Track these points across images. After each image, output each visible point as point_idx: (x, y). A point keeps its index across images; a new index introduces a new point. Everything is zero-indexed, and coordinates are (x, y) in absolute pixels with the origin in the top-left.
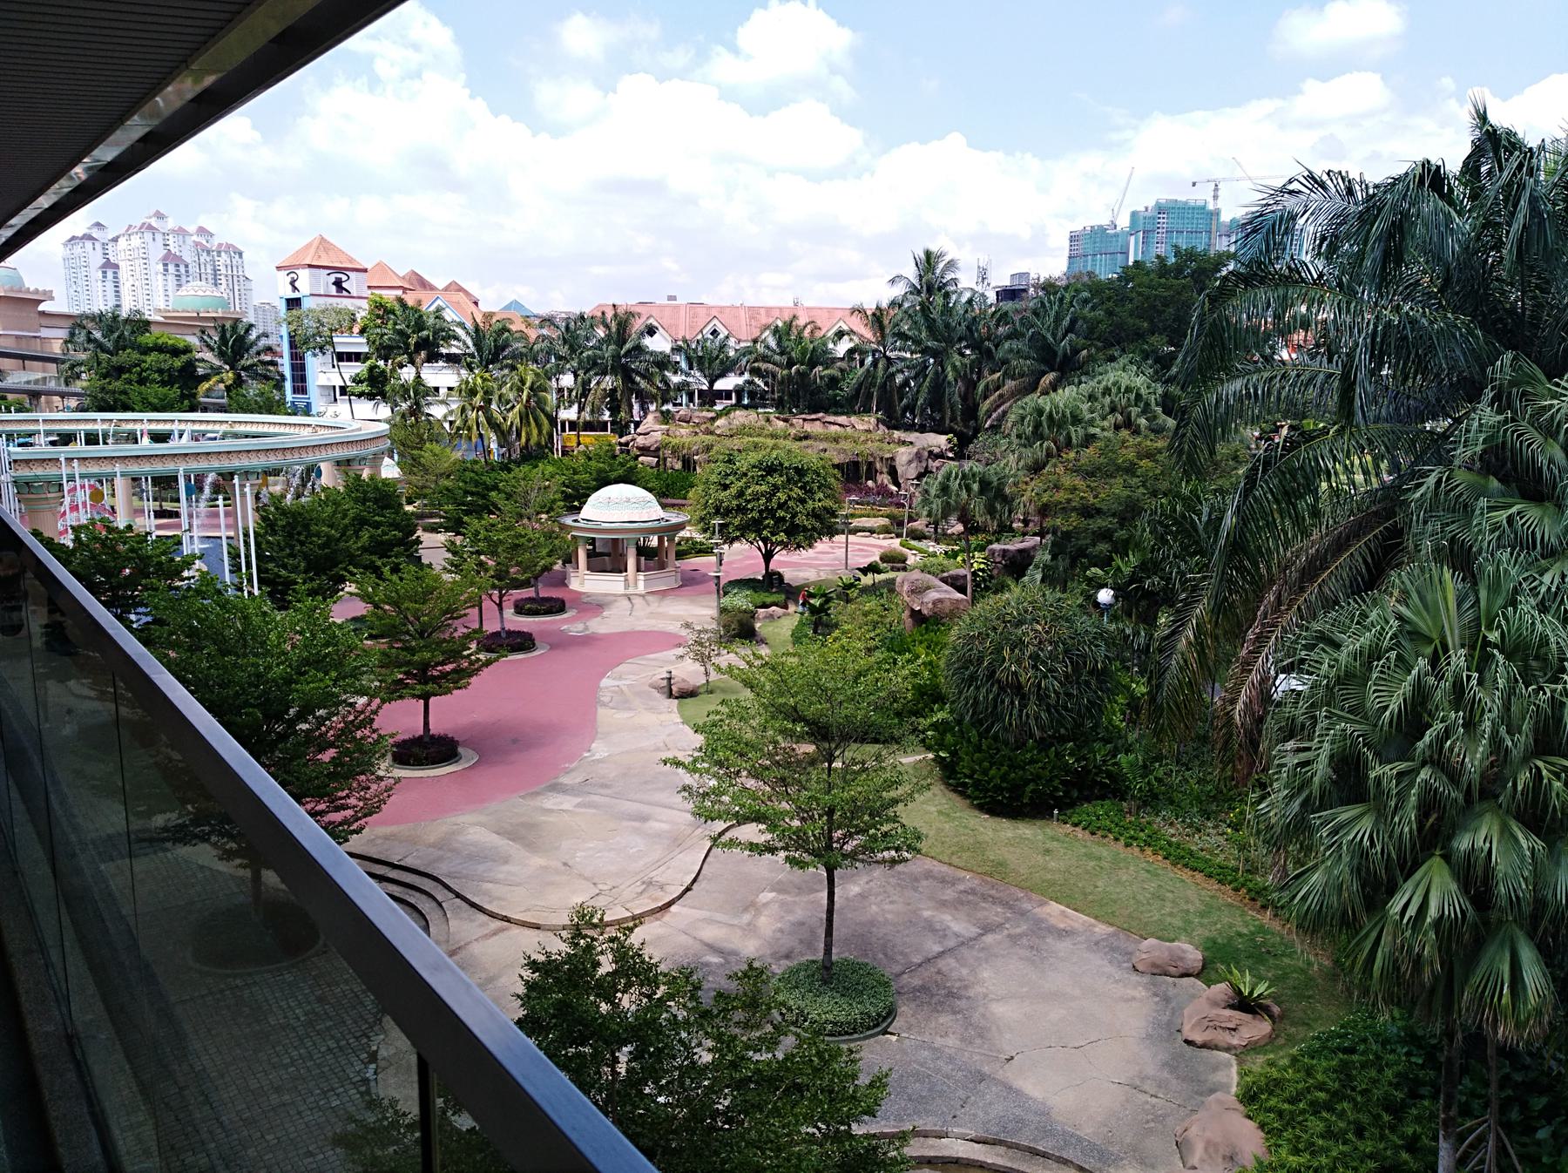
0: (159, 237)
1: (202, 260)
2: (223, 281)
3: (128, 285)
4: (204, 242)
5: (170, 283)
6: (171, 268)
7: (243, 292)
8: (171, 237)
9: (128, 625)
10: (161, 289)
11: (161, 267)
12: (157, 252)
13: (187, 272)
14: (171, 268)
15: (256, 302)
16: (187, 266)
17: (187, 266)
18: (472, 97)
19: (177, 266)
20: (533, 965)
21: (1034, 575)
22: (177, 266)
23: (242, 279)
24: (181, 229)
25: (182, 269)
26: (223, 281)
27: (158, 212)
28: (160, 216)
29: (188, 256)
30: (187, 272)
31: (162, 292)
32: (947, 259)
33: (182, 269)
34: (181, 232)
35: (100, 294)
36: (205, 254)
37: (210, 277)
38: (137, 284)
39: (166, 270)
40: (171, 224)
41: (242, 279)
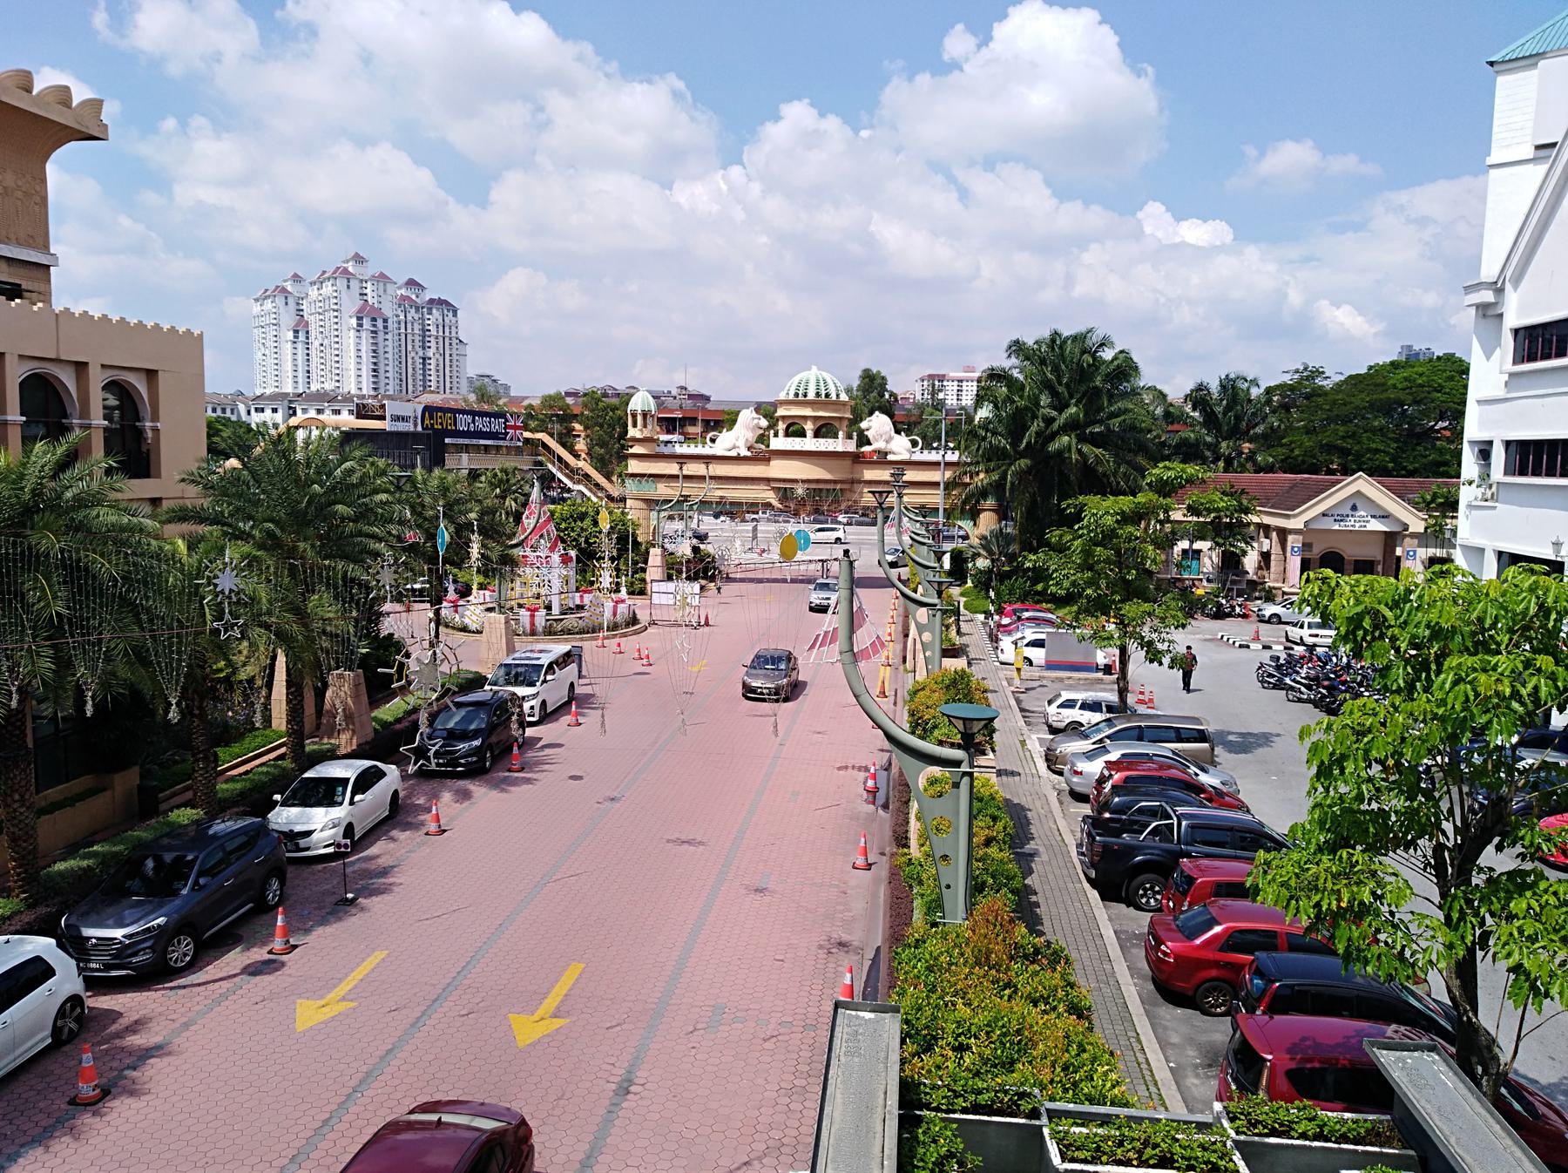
0: (354, 284)
1: (409, 318)
2: (433, 344)
3: (316, 344)
4: (414, 297)
5: (364, 341)
6: (367, 323)
7: (455, 357)
8: (369, 284)
9: (1293, 1138)
10: (352, 348)
11: (354, 322)
12: (351, 305)
13: (386, 327)
14: (367, 323)
15: (472, 371)
16: (385, 321)
17: (385, 321)
18: (822, 115)
19: (374, 319)
20: (201, 336)
21: (1474, 485)
22: (374, 319)
23: (455, 341)
24: (382, 275)
25: (380, 323)
26: (433, 344)
27: (357, 255)
28: (358, 259)
29: (388, 310)
30: (386, 327)
31: (353, 354)
32: (1214, 387)
33: (380, 323)
34: (382, 278)
35: (289, 357)
36: (413, 311)
37: (417, 338)
38: (326, 342)
39: (360, 325)
40: (371, 270)
41: (455, 341)
